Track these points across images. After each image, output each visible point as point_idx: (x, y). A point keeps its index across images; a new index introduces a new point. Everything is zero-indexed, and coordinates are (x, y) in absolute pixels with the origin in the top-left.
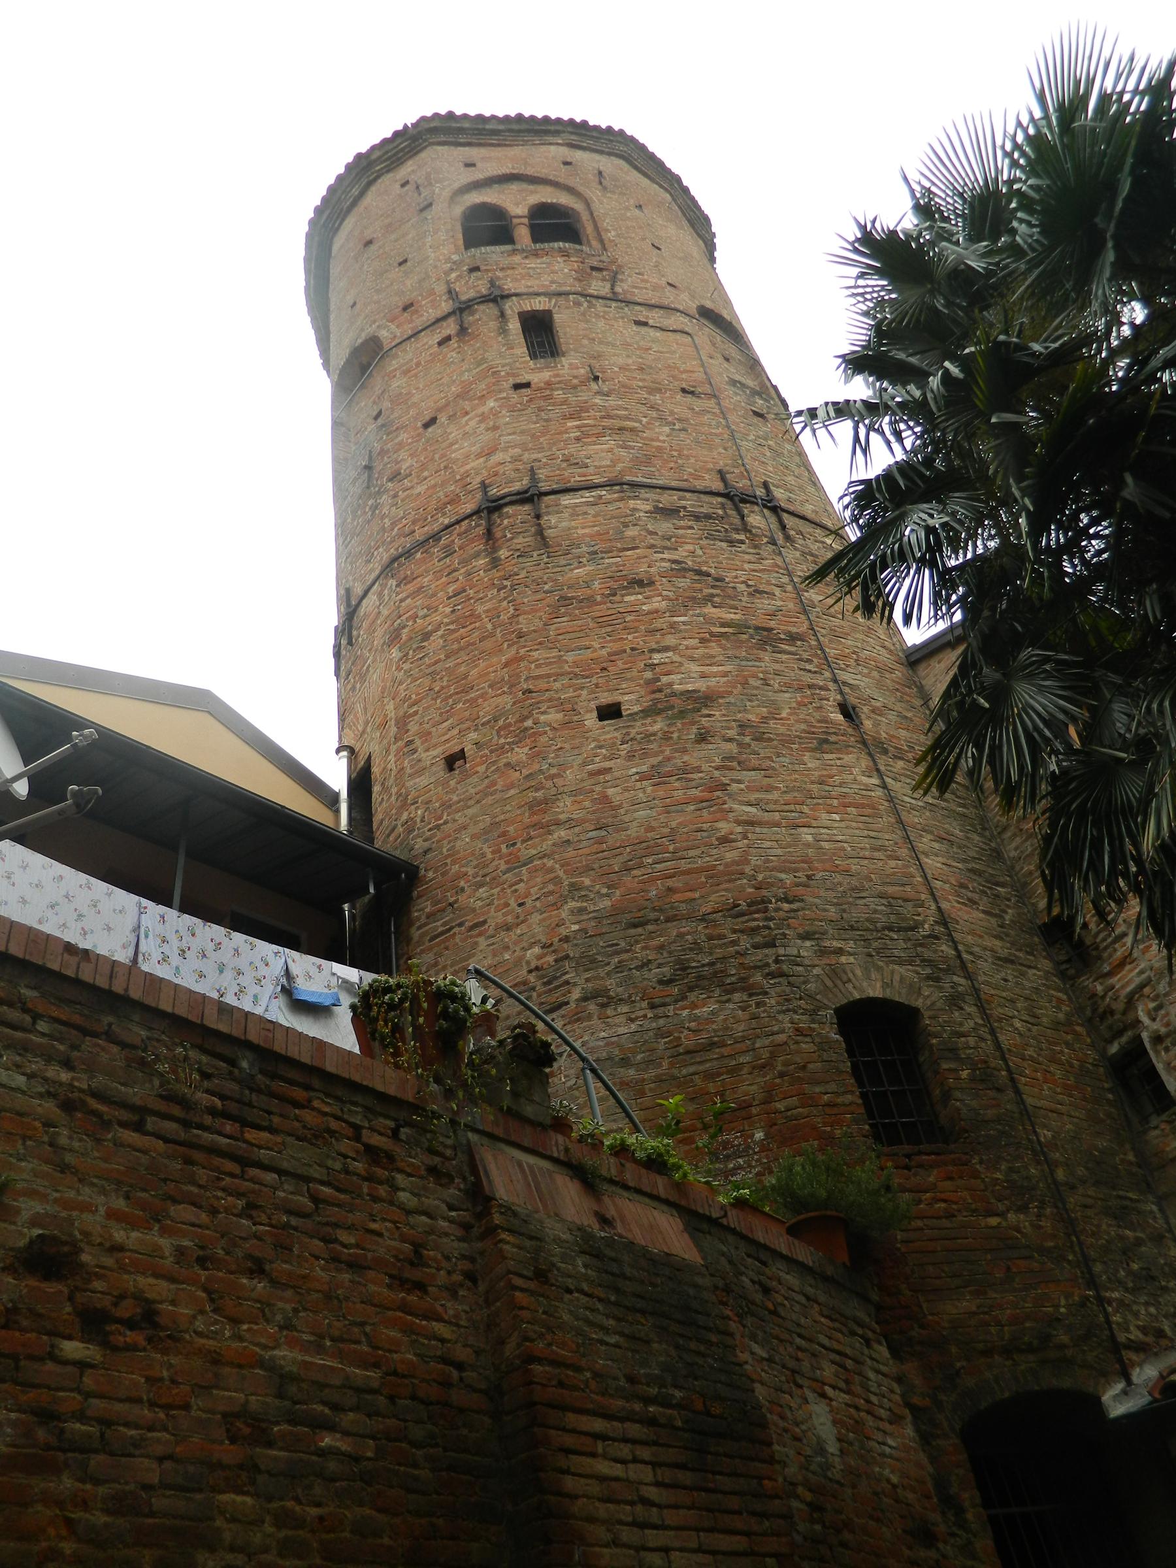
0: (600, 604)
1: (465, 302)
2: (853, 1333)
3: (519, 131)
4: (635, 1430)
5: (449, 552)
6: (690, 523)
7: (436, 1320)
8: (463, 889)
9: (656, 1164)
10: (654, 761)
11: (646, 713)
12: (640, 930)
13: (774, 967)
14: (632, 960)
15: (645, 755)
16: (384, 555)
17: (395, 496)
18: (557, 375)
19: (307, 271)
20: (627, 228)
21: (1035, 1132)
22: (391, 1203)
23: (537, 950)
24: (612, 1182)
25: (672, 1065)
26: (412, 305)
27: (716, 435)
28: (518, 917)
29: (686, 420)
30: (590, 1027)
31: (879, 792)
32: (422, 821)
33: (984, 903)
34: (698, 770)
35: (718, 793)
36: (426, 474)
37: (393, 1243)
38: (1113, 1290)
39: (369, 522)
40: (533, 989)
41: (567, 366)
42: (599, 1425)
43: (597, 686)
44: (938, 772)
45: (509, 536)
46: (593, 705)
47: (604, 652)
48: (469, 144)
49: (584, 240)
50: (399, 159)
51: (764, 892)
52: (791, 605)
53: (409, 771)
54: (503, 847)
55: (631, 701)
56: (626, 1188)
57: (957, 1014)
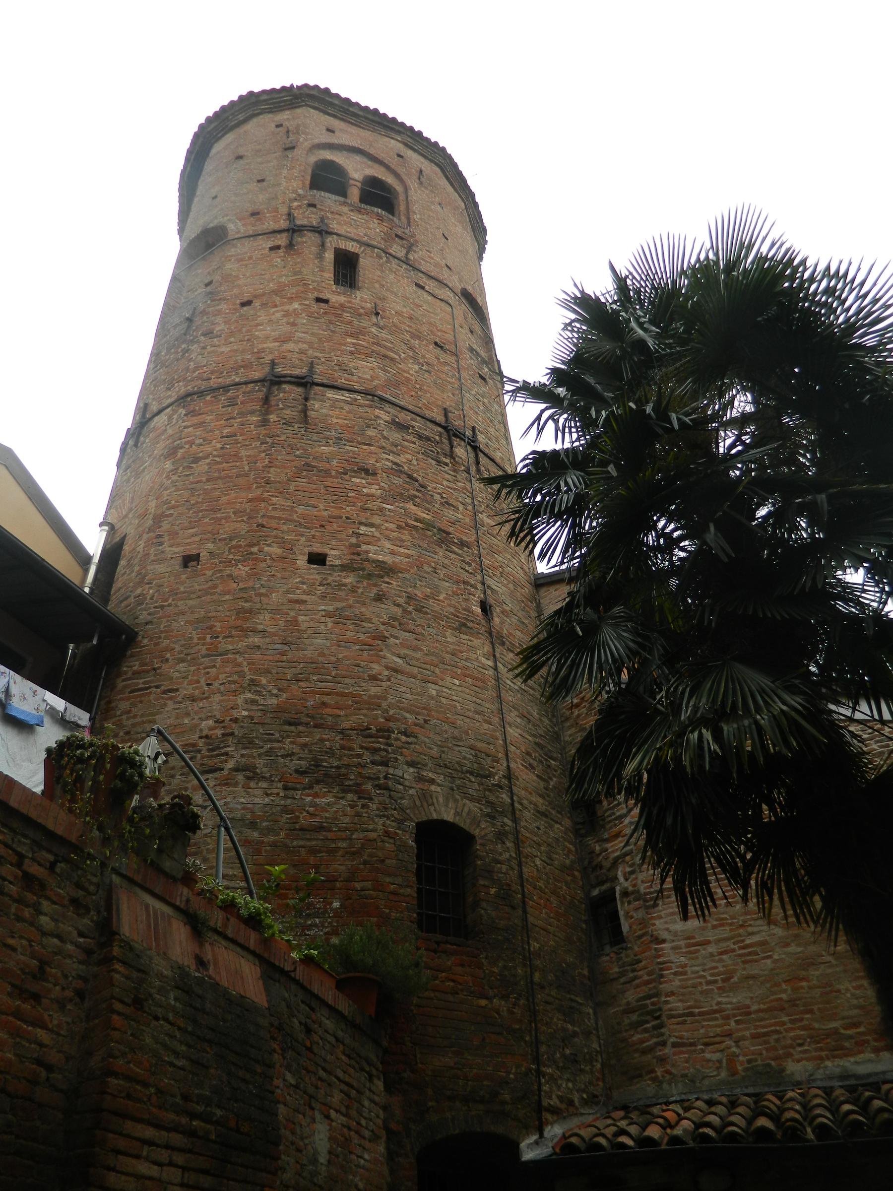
0: (332, 477)
1: (298, 226)
2: (362, 1069)
3: (373, 121)
4: (177, 1139)
5: (232, 403)
6: (414, 439)
7: (41, 1028)
8: (167, 660)
9: (254, 921)
10: (340, 605)
11: (344, 567)
12: (293, 728)
13: (382, 781)
14: (281, 749)
15: (334, 599)
16: (181, 388)
17: (204, 348)
18: (350, 302)
19: (187, 159)
20: (429, 216)
21: (528, 943)
22: (32, 924)
23: (211, 722)
24: (215, 931)
25: (287, 835)
26: (258, 213)
27: (449, 382)
28: (204, 693)
29: (433, 365)
30: (234, 792)
31: (491, 672)
32: (151, 599)
33: (539, 769)
34: (369, 621)
35: (379, 642)
36: (232, 339)
37: (22, 958)
38: (548, 1066)
39: (178, 360)
40: (199, 751)
41: (359, 298)
42: (149, 1133)
43: (313, 537)
44: (530, 661)
45: (281, 406)
46: (307, 550)
47: (326, 514)
48: (335, 116)
49: (397, 213)
50: (281, 107)
51: (391, 724)
52: (467, 520)
53: (152, 557)
54: (208, 637)
55: (335, 556)
56: (226, 937)
57: (499, 846)
